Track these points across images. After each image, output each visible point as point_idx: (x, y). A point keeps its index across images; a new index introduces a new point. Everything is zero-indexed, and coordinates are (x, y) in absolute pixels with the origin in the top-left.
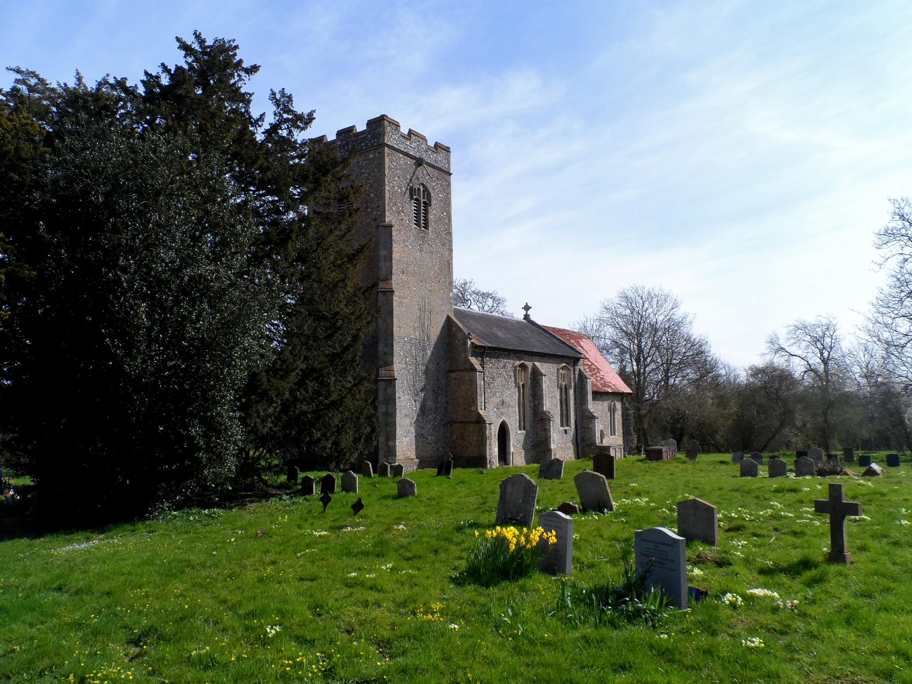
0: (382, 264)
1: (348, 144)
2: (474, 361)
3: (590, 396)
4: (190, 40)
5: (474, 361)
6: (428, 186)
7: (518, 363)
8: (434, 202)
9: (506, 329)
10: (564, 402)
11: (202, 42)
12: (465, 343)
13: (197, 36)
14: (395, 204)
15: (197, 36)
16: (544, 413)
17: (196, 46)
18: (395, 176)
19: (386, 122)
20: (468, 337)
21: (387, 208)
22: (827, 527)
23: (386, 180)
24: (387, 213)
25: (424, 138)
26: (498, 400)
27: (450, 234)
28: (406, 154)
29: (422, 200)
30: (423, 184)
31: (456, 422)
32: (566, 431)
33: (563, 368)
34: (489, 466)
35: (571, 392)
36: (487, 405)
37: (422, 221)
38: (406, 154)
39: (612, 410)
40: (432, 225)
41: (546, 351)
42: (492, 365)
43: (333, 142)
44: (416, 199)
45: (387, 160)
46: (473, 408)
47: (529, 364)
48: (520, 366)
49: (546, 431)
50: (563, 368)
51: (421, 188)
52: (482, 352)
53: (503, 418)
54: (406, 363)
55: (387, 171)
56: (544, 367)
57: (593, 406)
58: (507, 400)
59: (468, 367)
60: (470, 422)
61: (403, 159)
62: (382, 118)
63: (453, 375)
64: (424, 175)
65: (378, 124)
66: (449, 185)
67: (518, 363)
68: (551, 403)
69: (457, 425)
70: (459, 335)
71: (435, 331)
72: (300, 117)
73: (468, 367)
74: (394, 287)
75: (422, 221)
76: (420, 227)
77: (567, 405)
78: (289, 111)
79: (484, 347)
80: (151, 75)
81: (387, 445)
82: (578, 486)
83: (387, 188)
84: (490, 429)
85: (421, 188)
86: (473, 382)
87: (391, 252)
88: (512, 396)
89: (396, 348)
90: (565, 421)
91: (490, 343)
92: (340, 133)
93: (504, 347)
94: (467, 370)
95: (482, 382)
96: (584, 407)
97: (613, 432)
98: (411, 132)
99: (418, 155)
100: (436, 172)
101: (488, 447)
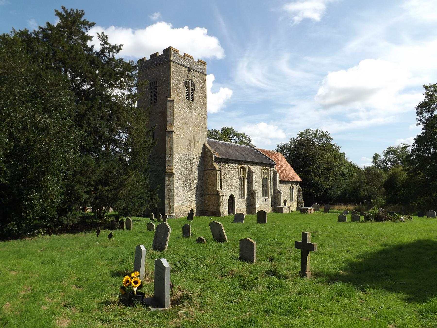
0: (168, 118)
1: (155, 61)
2: (216, 165)
3: (278, 183)
4: (61, 10)
5: (216, 165)
6: (194, 81)
7: (240, 166)
8: (197, 88)
9: (236, 150)
10: (265, 186)
11: (66, 11)
12: (212, 157)
13: (63, 8)
14: (176, 89)
15: (63, 8)
16: (253, 190)
17: (63, 13)
18: (177, 76)
19: (171, 50)
20: (212, 154)
21: (171, 91)
22: (300, 255)
23: (171, 78)
24: (172, 94)
25: (192, 58)
26: (229, 184)
27: (206, 104)
28: (183, 65)
29: (191, 88)
30: (191, 80)
31: (207, 195)
32: (265, 199)
33: (264, 169)
34: (221, 216)
35: (246, 180)
36: (223, 187)
37: (191, 97)
38: (183, 65)
39: (292, 189)
40: (196, 99)
41: (256, 161)
42: (226, 168)
43: (149, 60)
44: (187, 87)
45: (172, 68)
46: (215, 188)
47: (246, 167)
48: (241, 168)
49: (254, 199)
50: (264, 169)
51: (190, 82)
52: (219, 161)
53: (232, 193)
54: (181, 166)
55: (171, 73)
56: (253, 168)
57: (280, 187)
58: (234, 184)
59: (213, 168)
60: (213, 195)
61: (183, 68)
62: (170, 48)
63: (206, 172)
64: (194, 76)
65: (167, 51)
66: (205, 80)
67: (240, 166)
68: (257, 186)
69: (208, 196)
70: (209, 153)
71: (198, 152)
72: (115, 47)
73: (213, 168)
74: (174, 129)
75: (191, 97)
76: (189, 100)
77: (267, 187)
78: (107, 44)
79: (221, 159)
80: (42, 29)
81: (170, 205)
82: (211, 228)
83: (171, 82)
84: (223, 198)
85: (190, 82)
86: (215, 175)
87: (173, 113)
88: (237, 182)
89: (175, 159)
90: (265, 194)
91: (226, 157)
92: (151, 56)
93: (232, 158)
94: (212, 170)
95: (220, 176)
96: (276, 188)
97: (292, 200)
98: (185, 55)
99: (188, 66)
100: (198, 74)
101: (221, 207)
